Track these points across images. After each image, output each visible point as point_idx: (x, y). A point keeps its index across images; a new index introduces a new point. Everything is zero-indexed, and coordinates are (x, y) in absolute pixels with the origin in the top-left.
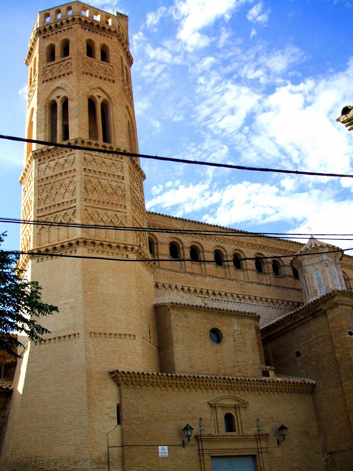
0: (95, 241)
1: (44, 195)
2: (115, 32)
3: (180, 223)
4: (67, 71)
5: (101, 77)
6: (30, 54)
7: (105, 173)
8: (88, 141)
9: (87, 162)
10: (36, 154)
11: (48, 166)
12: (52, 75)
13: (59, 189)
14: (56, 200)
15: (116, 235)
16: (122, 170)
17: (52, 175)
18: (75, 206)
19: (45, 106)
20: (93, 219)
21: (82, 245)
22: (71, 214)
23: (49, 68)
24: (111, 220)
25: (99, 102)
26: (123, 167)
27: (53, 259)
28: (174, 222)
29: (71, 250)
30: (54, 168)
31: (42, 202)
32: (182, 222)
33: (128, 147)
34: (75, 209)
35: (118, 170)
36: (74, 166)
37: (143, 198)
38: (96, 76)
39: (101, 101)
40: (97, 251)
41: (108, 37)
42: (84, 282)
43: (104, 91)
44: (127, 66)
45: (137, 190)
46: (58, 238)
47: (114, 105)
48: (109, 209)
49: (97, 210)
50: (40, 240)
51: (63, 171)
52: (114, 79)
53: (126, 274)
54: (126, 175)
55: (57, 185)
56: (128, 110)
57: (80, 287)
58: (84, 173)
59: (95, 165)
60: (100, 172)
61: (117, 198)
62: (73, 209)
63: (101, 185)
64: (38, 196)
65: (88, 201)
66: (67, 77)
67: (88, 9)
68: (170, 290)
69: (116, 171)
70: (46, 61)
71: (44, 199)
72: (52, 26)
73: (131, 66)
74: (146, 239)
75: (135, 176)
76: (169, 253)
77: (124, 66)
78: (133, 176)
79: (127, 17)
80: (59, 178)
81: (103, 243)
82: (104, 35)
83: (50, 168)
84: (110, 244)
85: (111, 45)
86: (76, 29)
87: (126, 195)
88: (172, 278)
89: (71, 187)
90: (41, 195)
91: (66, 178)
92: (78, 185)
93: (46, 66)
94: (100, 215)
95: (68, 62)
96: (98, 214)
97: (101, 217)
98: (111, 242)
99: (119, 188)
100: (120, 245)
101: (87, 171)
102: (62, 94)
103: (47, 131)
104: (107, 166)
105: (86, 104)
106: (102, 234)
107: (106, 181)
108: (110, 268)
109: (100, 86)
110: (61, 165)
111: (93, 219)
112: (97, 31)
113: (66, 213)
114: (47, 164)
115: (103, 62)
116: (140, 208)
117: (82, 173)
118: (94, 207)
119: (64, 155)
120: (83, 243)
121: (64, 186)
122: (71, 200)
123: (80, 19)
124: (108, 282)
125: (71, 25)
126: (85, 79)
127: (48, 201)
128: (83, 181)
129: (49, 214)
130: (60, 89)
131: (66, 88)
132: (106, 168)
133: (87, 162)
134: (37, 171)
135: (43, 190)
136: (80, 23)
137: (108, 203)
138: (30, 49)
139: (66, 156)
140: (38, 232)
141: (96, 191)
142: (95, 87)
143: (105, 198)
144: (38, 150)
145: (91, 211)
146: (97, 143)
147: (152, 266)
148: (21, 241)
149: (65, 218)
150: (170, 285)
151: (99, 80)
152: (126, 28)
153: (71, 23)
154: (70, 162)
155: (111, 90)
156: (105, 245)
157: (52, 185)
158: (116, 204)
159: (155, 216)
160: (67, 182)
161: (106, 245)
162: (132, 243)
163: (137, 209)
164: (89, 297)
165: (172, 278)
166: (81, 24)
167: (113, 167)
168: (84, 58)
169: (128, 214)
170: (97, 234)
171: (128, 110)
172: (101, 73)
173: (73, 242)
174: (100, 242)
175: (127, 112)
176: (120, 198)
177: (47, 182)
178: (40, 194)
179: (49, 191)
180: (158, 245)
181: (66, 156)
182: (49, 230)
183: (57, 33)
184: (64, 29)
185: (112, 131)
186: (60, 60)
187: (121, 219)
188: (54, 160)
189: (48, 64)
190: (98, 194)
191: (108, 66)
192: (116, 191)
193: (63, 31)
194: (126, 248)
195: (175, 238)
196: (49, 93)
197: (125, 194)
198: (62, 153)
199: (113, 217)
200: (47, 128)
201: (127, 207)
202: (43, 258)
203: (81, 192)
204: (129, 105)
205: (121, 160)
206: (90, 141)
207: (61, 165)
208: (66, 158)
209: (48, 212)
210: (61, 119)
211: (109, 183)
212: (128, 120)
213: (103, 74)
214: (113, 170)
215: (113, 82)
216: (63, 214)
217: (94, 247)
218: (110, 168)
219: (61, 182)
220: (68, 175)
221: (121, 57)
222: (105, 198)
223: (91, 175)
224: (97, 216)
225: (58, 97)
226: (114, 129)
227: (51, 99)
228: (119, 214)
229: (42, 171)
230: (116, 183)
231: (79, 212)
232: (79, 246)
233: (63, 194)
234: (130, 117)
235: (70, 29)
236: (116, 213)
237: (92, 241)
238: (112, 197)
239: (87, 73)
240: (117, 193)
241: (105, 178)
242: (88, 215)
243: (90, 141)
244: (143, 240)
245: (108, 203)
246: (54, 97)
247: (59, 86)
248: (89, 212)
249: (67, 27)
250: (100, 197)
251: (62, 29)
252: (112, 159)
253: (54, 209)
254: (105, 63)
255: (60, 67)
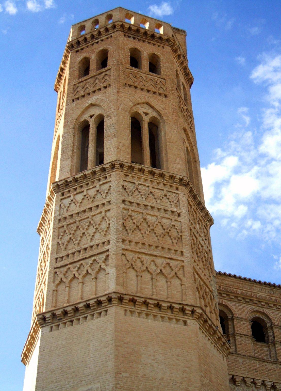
0: (136, 298)
1: (66, 238)
2: (168, 40)
3: (266, 289)
4: (104, 84)
5: (148, 91)
6: (60, 76)
7: (152, 207)
8: (130, 165)
9: (127, 192)
10: (58, 186)
11: (74, 200)
12: (84, 91)
13: (87, 229)
14: (81, 244)
15: (168, 291)
16: (178, 203)
17: (78, 211)
18: (108, 250)
19: (74, 128)
20: (134, 268)
21: (116, 302)
22: (101, 261)
23: (81, 84)
24: (161, 270)
25: (146, 119)
26: (178, 201)
27: (74, 325)
28: (257, 288)
29: (100, 311)
30: (81, 202)
31: (63, 247)
32: (269, 288)
33: (185, 175)
34: (107, 253)
35: (172, 203)
36: (108, 197)
37: (209, 248)
38: (142, 89)
39: (149, 119)
40: (139, 313)
41: (159, 46)
42: (117, 357)
43: (152, 107)
44: (184, 83)
45: (200, 236)
46: (82, 295)
47: (166, 123)
48: (157, 255)
49: (140, 256)
50: (56, 300)
51: (92, 205)
52: (167, 94)
53: (184, 348)
54: (184, 210)
55: (85, 224)
56: (187, 135)
57: (111, 365)
58: (123, 206)
59: (139, 196)
60: (145, 206)
61: (171, 241)
62: (105, 254)
63: (147, 223)
64: (57, 240)
65: (127, 242)
66: (103, 91)
67: (132, 16)
68: (254, 389)
69: (169, 206)
70: (78, 77)
71: (66, 243)
72: (87, 37)
73: (190, 86)
74: (214, 304)
75: (203, 250)
76: (250, 332)
77: (181, 84)
78: (195, 216)
79: (184, 32)
80: (88, 214)
81: (148, 301)
82: (154, 45)
83: (76, 203)
84: (158, 303)
85: (162, 54)
86: (117, 37)
87: (183, 237)
88: (256, 370)
89: (104, 226)
90: (61, 238)
91: (97, 214)
92: (113, 222)
93: (77, 83)
94: (145, 262)
95: (106, 74)
96: (142, 262)
97: (146, 265)
98: (160, 300)
99: (173, 227)
100: (173, 305)
101: (127, 203)
102: (96, 112)
103: (75, 158)
104: (155, 199)
105: (128, 122)
106: (146, 290)
107: (154, 218)
108: (159, 339)
109: (147, 100)
110: (91, 198)
111: (134, 268)
112: (144, 39)
113: (95, 260)
114: (72, 198)
115: (151, 73)
116: (206, 260)
117: (120, 205)
118: (135, 252)
119: (95, 185)
120: (117, 300)
121: (94, 225)
122: (103, 241)
123: (122, 26)
124: (154, 360)
125: (111, 34)
126: (127, 92)
127: (71, 246)
128: (120, 217)
129: (71, 263)
130: (94, 107)
131: (101, 104)
132: (154, 201)
133: (127, 192)
134: (59, 208)
135: (65, 231)
136: (122, 30)
137: (157, 247)
138: (61, 70)
139: (98, 186)
140: (55, 288)
141: (140, 230)
142: (140, 101)
143: (153, 239)
144: (60, 181)
145: (131, 257)
146: (142, 168)
147: (224, 343)
148: (34, 309)
149: (93, 267)
150: (254, 379)
151: (146, 93)
152: (183, 43)
153: (111, 31)
154: (104, 193)
155: (162, 106)
156: (151, 304)
157: (77, 224)
158: (169, 249)
159: (228, 280)
160: (98, 219)
161: (153, 304)
162: (193, 304)
163: (200, 260)
164: (124, 381)
165: (256, 370)
166: (123, 31)
167: (165, 200)
168: (126, 68)
169: (186, 264)
170: (139, 289)
171: (187, 135)
172: (149, 85)
173: (102, 299)
174: (143, 300)
175: (184, 137)
176: (175, 241)
177: (71, 221)
178: (60, 237)
179: (73, 232)
180: (235, 321)
181: (98, 186)
182: (70, 285)
183: (93, 45)
184: (102, 39)
185: (164, 155)
186: (95, 74)
187: (176, 270)
188: (83, 192)
189: (80, 80)
190: (142, 234)
191: (159, 79)
192: (168, 231)
193: (101, 41)
194: (183, 310)
195: (259, 312)
196: (80, 112)
197: (181, 236)
198: (93, 182)
199: (163, 266)
200: (75, 154)
201: (185, 254)
202: (59, 325)
203: (117, 230)
204: (187, 128)
205: (176, 192)
206: (131, 166)
207: (91, 198)
208: (98, 188)
209: (70, 260)
210: (94, 141)
211: (158, 221)
212: (187, 148)
213: (151, 87)
214: (166, 204)
215: (166, 96)
216: (91, 262)
217: (135, 306)
218: (160, 200)
219: (89, 220)
220: (99, 210)
221: (177, 71)
222: (153, 239)
223: (133, 208)
224: (139, 264)
225: (91, 117)
226: (166, 153)
227: (82, 120)
228: (172, 263)
229: (65, 207)
230: (170, 221)
231: (114, 257)
232: (111, 304)
233: (93, 234)
234: (190, 143)
235: (109, 38)
236: (168, 261)
237: (131, 297)
238: (163, 239)
239: (130, 86)
240: (170, 234)
241: (153, 214)
242: (126, 262)
243: (131, 166)
244: (210, 305)
245: (157, 247)
246: (86, 117)
247: (93, 103)
248: (128, 258)
249: (106, 37)
250: (146, 239)
251: (100, 39)
252: (163, 190)
253: (79, 256)
254: (154, 74)
255: (95, 80)
